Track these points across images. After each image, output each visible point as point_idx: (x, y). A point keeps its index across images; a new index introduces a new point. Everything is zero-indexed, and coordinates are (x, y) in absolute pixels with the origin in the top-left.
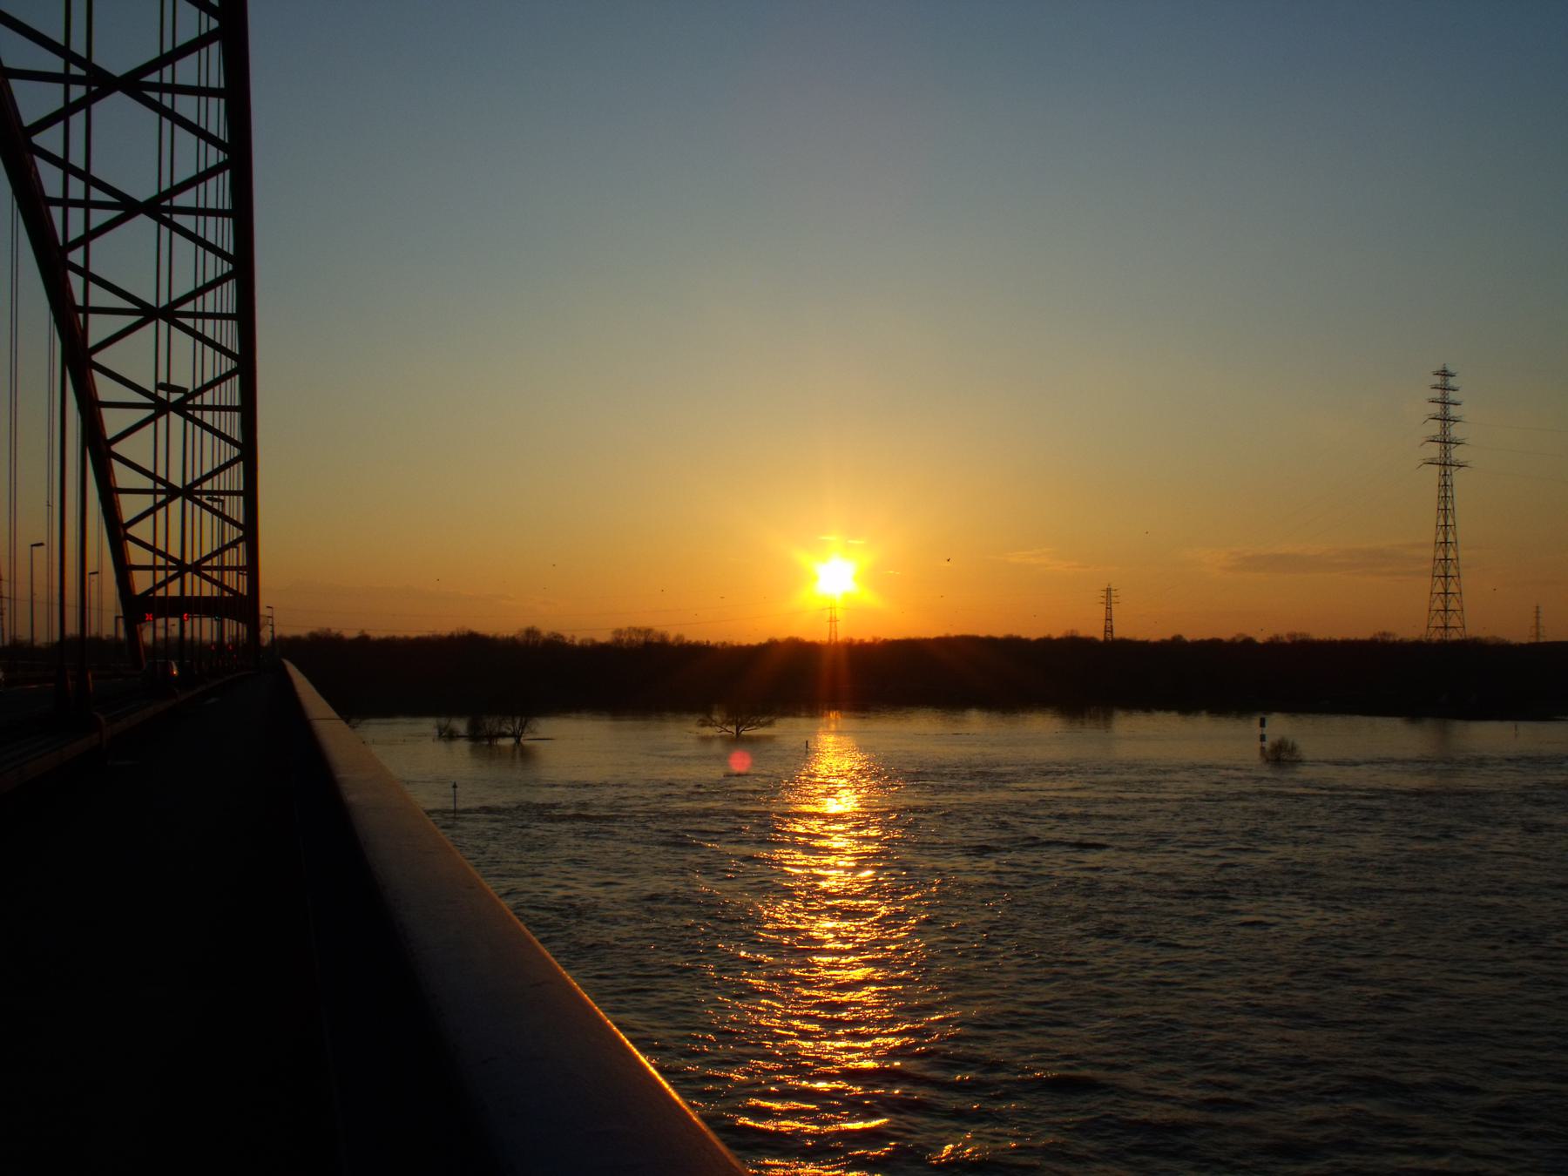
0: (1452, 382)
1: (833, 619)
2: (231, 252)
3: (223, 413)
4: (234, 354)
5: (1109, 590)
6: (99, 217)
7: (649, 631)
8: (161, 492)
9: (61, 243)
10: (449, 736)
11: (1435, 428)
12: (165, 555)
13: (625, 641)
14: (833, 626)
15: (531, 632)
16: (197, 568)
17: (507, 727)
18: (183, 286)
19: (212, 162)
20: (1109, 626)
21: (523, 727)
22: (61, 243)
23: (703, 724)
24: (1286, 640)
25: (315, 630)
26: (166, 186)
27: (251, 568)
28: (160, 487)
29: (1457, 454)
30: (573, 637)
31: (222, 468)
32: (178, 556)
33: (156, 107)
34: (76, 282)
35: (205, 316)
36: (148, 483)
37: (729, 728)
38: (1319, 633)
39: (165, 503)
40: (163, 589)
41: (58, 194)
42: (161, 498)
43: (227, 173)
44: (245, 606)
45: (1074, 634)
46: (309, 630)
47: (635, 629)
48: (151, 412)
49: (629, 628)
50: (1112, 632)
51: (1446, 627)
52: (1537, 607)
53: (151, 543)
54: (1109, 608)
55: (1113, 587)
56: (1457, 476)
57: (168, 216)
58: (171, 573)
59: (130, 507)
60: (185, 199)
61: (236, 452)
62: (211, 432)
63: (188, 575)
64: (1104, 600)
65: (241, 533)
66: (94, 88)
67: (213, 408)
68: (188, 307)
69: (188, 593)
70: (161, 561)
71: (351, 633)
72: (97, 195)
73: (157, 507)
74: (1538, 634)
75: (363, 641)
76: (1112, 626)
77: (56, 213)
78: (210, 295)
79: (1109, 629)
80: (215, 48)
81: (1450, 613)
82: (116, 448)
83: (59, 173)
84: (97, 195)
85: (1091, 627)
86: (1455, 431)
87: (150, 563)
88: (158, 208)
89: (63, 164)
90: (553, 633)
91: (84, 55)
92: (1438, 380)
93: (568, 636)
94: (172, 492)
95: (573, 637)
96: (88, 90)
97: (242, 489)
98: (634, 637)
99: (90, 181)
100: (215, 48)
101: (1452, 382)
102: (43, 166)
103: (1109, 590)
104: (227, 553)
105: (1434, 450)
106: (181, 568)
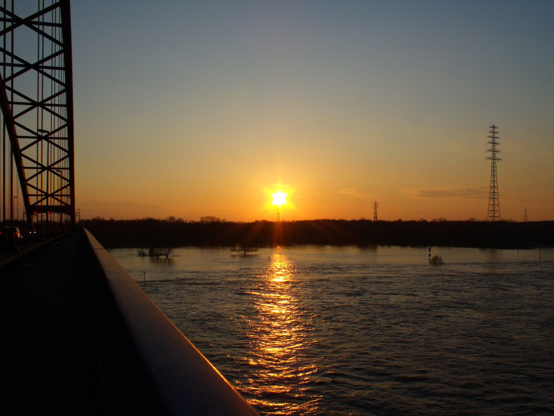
0: (496, 130)
1: (278, 213)
2: (64, 83)
4: (66, 119)
5: (376, 203)
6: (17, 70)
7: (213, 218)
8: (40, 168)
9: (3, 79)
10: (142, 255)
11: (490, 146)
12: (41, 191)
13: (205, 221)
14: (278, 215)
15: (171, 218)
16: (52, 195)
17: (163, 252)
18: (47, 95)
19: (57, 50)
20: (376, 216)
21: (169, 251)
22: (3, 79)
23: (233, 250)
24: (438, 221)
25: (95, 217)
26: (41, 59)
27: (72, 195)
28: (39, 166)
29: (498, 155)
30: (187, 220)
31: (61, 160)
32: (46, 191)
35: (55, 105)
36: (35, 165)
37: (241, 252)
38: (450, 218)
39: (41, 172)
42: (39, 170)
43: (67, 127)
44: (70, 209)
45: (363, 219)
46: (92, 218)
47: (208, 217)
48: (36, 140)
49: (206, 217)
50: (377, 218)
51: (494, 216)
52: (526, 209)
54: (376, 210)
55: (377, 202)
56: (498, 163)
57: (41, 69)
58: (43, 197)
59: (28, 173)
60: (48, 63)
61: (61, 48)
63: (49, 198)
64: (374, 207)
65: (68, 183)
66: (14, 23)
67: (58, 138)
68: (49, 102)
69: (49, 204)
70: (40, 193)
71: (107, 218)
72: (16, 62)
73: (38, 173)
74: (526, 219)
75: (112, 221)
76: (377, 216)
78: (57, 98)
79: (376, 217)
80: (58, 9)
81: (495, 211)
82: (23, 152)
84: (16, 62)
85: (370, 217)
86: (497, 147)
87: (36, 194)
88: (38, 67)
90: (179, 218)
92: (491, 129)
93: (185, 219)
94: (43, 168)
95: (187, 220)
97: (68, 167)
98: (208, 220)
99: (13, 57)
100: (58, 9)
101: (496, 130)
103: (376, 203)
105: (490, 154)
106: (47, 195)
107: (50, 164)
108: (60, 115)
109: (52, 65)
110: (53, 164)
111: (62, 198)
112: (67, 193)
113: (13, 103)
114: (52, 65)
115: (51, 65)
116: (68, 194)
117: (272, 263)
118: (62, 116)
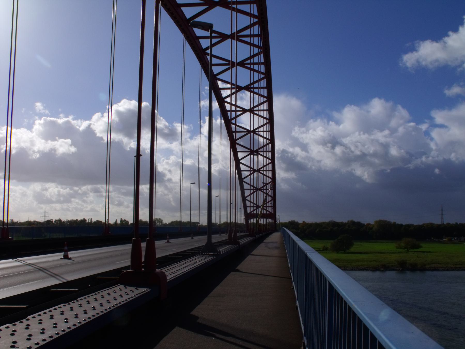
3: (266, 133)
4: (260, 46)
6: (239, 113)
8: (252, 171)
9: (230, 119)
12: (253, 186)
22: (230, 119)
26: (252, 81)
27: (275, 207)
31: (266, 165)
32: (256, 186)
33: (248, 68)
34: (233, 126)
35: (261, 110)
36: (249, 169)
39: (253, 173)
40: (254, 209)
41: (229, 109)
42: (252, 172)
44: (273, 216)
53: (249, 183)
58: (254, 191)
59: (247, 193)
60: (256, 85)
61: (267, 121)
62: (261, 116)
65: (269, 142)
66: (237, 90)
67: (263, 131)
68: (257, 108)
70: (252, 188)
72: (238, 109)
77: (229, 113)
82: (244, 180)
83: (249, 203)
84: (238, 109)
87: (249, 188)
88: (251, 111)
89: (250, 201)
91: (253, 185)
94: (254, 171)
96: (236, 90)
97: (269, 130)
102: (247, 202)
104: (267, 186)
107: (258, 168)
108: (264, 119)
109: (253, 5)
110: (260, 148)
111: (268, 209)
112: (270, 169)
113: (236, 132)
114: (253, 5)
115: (258, 86)
116: (271, 170)
117: (363, 268)
118: (266, 137)
